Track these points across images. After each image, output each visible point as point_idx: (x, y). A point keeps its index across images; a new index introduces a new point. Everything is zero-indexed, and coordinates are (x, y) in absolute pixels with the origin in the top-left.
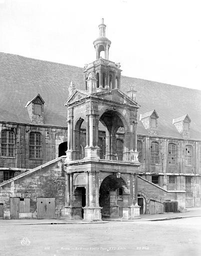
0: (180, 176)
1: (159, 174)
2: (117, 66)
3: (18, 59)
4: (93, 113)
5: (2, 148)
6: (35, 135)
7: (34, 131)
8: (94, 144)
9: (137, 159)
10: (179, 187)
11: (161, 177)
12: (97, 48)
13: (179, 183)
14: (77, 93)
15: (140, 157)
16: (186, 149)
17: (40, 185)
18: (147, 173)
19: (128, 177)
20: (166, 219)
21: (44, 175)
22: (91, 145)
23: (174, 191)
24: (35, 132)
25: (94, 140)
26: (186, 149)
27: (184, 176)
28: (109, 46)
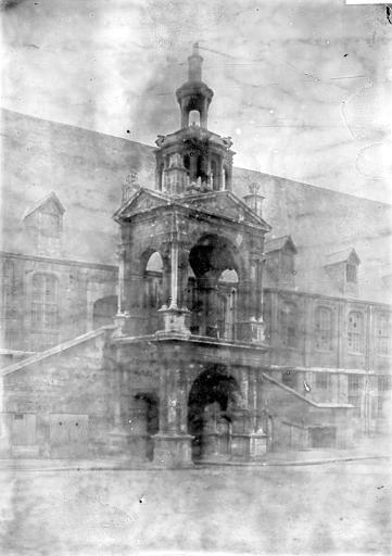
0: (337, 374)
1: (298, 368)
2: (225, 143)
3: (300, 196)
4: (178, 238)
5: (11, 314)
6: (44, 279)
7: (42, 271)
8: (180, 302)
9: (263, 337)
10: (334, 400)
11: (301, 376)
12: (185, 102)
13: (335, 390)
14: (143, 195)
15: (269, 332)
16: (351, 320)
17: (58, 386)
18: (273, 367)
19: (244, 373)
20: (318, 463)
21: (65, 365)
22: (173, 305)
23: (330, 405)
24: (45, 274)
25: (181, 294)
26: (351, 320)
27: (346, 374)
28: (209, 101)
